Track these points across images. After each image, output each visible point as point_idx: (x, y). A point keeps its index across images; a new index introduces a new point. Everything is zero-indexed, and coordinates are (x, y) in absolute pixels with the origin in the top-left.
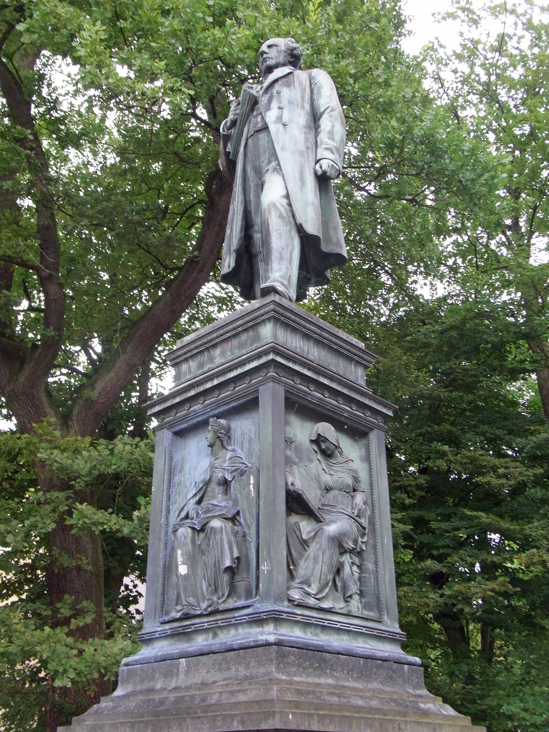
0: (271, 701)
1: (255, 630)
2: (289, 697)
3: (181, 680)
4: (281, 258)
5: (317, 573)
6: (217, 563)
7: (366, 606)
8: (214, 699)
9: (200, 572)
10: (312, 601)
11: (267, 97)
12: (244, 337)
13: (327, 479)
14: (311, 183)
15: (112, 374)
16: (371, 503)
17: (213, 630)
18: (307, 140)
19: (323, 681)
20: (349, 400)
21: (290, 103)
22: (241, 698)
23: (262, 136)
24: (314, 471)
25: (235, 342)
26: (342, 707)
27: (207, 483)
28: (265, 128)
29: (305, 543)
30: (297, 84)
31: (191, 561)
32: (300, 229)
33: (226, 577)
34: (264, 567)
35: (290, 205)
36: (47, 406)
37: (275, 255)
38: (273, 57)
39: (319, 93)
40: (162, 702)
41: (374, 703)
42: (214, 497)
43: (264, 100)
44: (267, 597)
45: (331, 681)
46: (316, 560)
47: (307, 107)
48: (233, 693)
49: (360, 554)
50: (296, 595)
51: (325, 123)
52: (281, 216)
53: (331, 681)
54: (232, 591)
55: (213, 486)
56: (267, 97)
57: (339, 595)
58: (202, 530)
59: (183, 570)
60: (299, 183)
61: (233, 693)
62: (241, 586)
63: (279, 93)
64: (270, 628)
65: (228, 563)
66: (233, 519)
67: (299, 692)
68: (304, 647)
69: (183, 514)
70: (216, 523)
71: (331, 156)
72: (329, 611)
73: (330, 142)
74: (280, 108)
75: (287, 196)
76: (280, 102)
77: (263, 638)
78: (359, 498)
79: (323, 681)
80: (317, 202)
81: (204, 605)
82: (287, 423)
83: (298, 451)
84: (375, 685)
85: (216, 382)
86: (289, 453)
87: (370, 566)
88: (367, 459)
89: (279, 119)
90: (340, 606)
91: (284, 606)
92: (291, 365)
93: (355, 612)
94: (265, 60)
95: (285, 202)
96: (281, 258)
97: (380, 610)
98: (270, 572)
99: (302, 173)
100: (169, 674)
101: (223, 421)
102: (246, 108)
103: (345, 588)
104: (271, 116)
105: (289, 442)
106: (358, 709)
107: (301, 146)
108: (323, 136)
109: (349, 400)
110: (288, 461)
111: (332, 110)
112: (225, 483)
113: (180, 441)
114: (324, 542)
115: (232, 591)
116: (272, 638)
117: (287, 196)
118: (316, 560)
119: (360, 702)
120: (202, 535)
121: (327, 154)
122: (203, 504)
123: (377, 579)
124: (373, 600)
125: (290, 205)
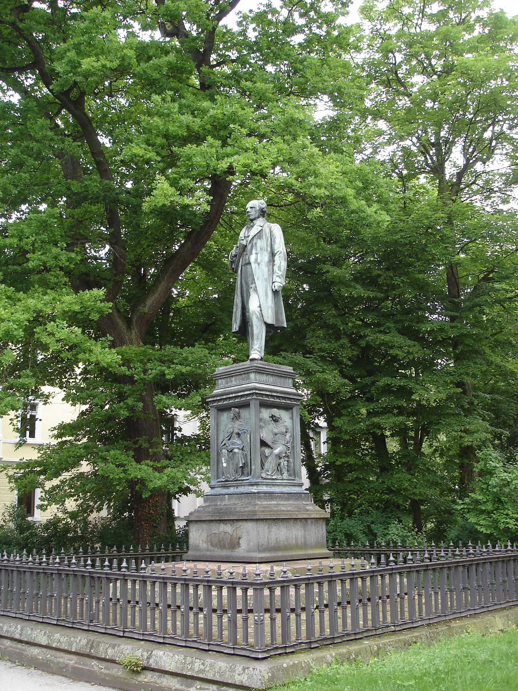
0: (256, 511)
1: (251, 487)
2: (262, 509)
3: (226, 502)
4: (258, 339)
5: (271, 467)
6: (237, 464)
7: (290, 475)
8: (238, 509)
9: (231, 466)
10: (269, 477)
11: (250, 245)
12: (244, 376)
13: (276, 431)
14: (270, 293)
15: (156, 295)
16: (293, 436)
17: (237, 486)
18: (269, 270)
19: (272, 503)
20: (284, 398)
21: (261, 249)
22: (247, 509)
23: (249, 267)
24: (271, 428)
25: (240, 377)
26: (277, 511)
27: (232, 433)
28: (249, 263)
29: (267, 457)
30: (264, 237)
31: (227, 462)
32: (266, 323)
33: (240, 470)
34: (253, 467)
35: (261, 310)
36: (117, 318)
37: (255, 337)
38: (253, 214)
39: (274, 241)
40: (221, 510)
41: (289, 509)
42: (234, 439)
43: (249, 247)
44: (254, 477)
45: (275, 502)
46: (271, 463)
47: (269, 249)
48: (244, 508)
49: (288, 456)
50: (264, 475)
51: (277, 258)
52: (257, 317)
53: (275, 502)
54: (243, 474)
55: (234, 434)
56: (250, 245)
57: (279, 473)
58: (231, 451)
59: (225, 465)
60: (265, 298)
61: (244, 508)
62: (245, 472)
63: (256, 244)
64: (255, 487)
65: (241, 465)
66: (242, 449)
67: (264, 507)
68: (265, 493)
69: (223, 444)
70: (236, 450)
71: (279, 280)
72: (275, 479)
73: (279, 272)
74: (256, 254)
75: (260, 306)
76: (256, 250)
77: (253, 491)
78: (288, 435)
79: (272, 503)
80: (273, 306)
81: (233, 478)
82: (260, 412)
83: (265, 423)
84: (291, 502)
85: (234, 395)
86: (261, 424)
87: (291, 460)
88: (292, 418)
89: (256, 260)
90: (279, 477)
91: (260, 480)
92: (261, 392)
93: (285, 477)
94: (249, 216)
95: (259, 309)
96: (258, 339)
97: (295, 476)
98: (255, 469)
99: (266, 291)
100: (222, 500)
101: (237, 410)
102: (241, 250)
103: (281, 471)
104: (253, 258)
105: (261, 420)
106: (283, 511)
107: (266, 276)
108: (276, 268)
109: (284, 398)
110: (261, 427)
111: (280, 253)
112: (238, 434)
113: (220, 413)
114: (274, 457)
115: (243, 474)
116: (256, 491)
117: (260, 306)
118: (271, 463)
119: (284, 509)
120: (231, 453)
121: (278, 279)
122: (231, 441)
123: (294, 464)
124: (292, 473)
125: (261, 310)
